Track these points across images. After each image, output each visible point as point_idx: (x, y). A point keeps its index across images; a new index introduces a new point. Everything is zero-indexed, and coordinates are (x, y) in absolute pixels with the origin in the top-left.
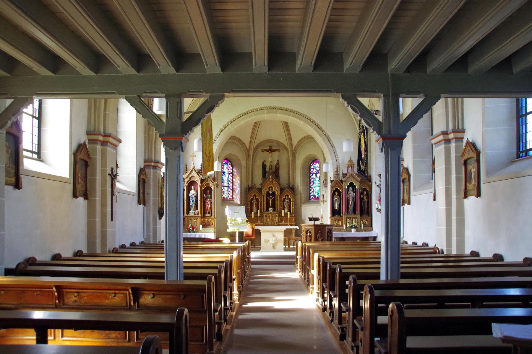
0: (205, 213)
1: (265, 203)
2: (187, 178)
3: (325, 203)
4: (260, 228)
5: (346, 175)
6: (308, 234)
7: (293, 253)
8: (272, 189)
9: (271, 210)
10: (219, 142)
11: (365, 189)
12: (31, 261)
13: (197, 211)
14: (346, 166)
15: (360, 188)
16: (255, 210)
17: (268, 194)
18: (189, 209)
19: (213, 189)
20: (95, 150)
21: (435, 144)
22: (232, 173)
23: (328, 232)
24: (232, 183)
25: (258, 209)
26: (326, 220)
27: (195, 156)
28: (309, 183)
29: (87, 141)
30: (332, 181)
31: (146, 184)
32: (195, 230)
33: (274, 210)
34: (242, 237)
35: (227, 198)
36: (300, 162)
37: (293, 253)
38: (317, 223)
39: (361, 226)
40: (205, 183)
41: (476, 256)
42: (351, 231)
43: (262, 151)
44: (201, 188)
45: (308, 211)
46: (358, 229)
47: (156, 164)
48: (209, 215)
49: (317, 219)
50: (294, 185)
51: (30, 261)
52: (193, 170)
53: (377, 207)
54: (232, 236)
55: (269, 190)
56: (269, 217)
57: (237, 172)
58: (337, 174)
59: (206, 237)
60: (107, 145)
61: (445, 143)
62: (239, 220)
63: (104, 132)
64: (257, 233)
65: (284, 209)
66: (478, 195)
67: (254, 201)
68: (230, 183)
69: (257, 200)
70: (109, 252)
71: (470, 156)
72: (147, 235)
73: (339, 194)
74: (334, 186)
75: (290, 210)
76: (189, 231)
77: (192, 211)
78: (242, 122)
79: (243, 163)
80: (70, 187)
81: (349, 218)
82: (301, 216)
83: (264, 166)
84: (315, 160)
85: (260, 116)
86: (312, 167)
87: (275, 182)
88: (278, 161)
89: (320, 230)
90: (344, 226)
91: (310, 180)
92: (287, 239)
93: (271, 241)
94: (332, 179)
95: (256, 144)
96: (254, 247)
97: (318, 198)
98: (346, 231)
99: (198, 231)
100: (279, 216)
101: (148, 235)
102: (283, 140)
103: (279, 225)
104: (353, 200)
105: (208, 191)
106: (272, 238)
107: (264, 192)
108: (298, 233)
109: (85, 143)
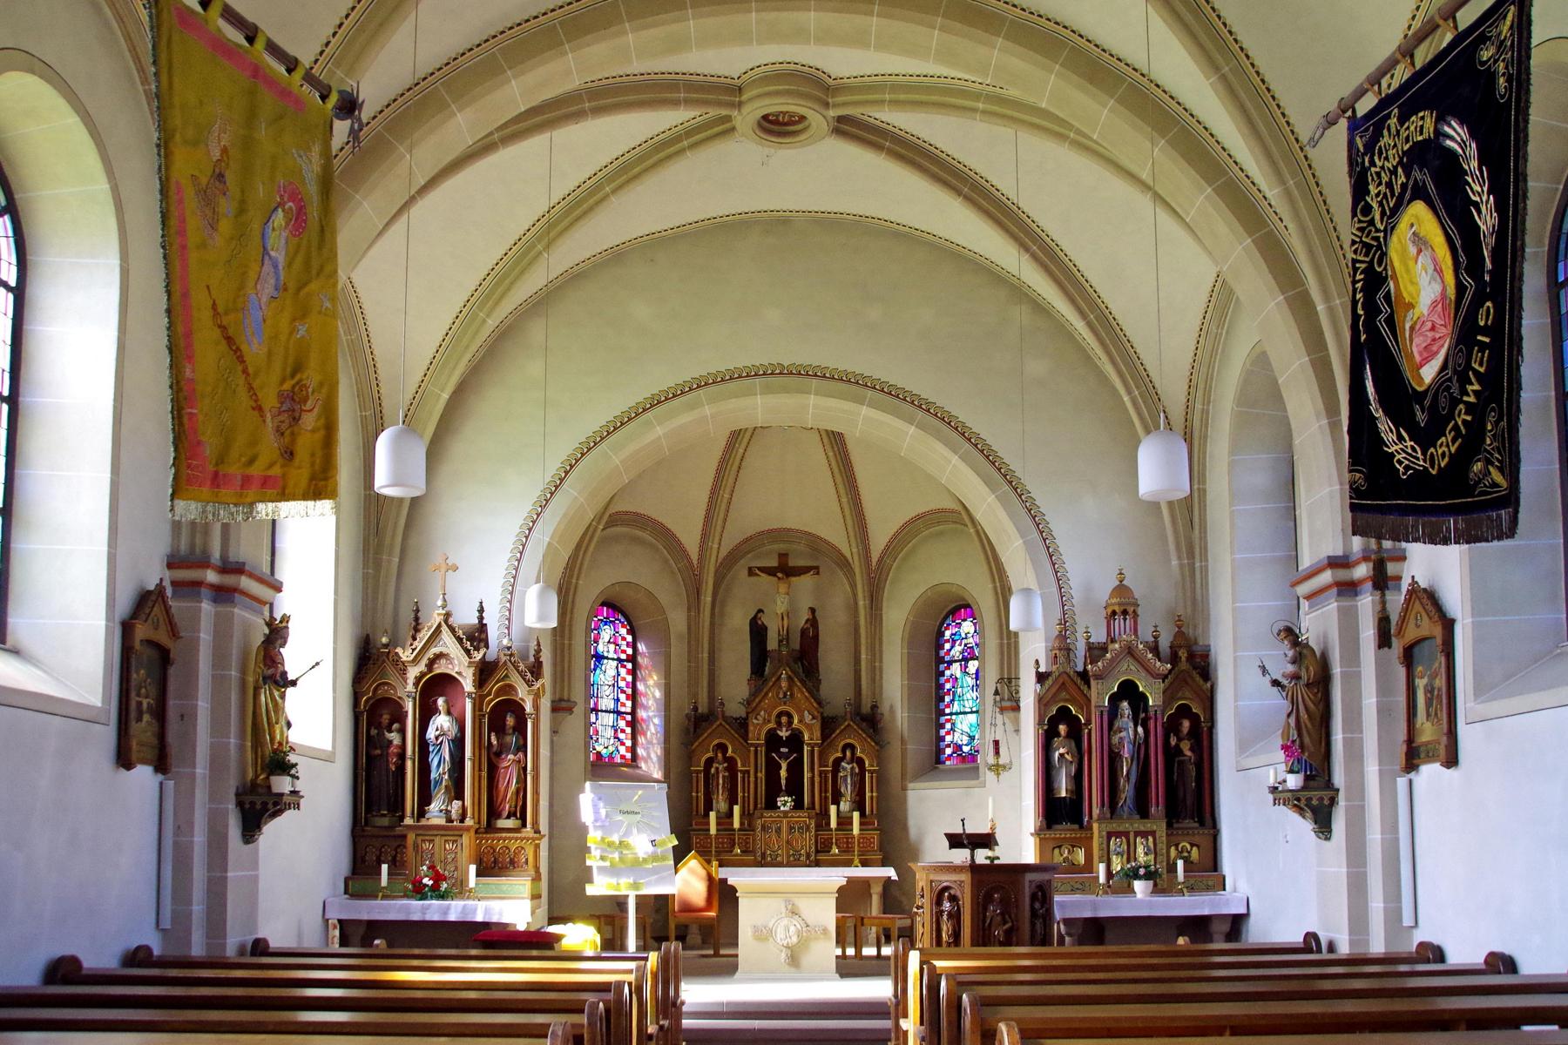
0: (494, 813)
1: (762, 775)
2: (415, 661)
3: (1004, 775)
4: (738, 878)
5: (1103, 649)
6: (947, 905)
7: (879, 989)
8: (790, 723)
9: (785, 802)
11: (1184, 711)
12: (63, 970)
13: (456, 804)
16: (721, 803)
17: (773, 741)
18: (425, 798)
19: (528, 708)
20: (195, 617)
21: (1308, 598)
22: (632, 659)
23: (1034, 897)
24: (634, 697)
25: (732, 801)
26: (1020, 843)
28: (934, 700)
29: (167, 584)
30: (1041, 678)
31: (172, 671)
32: (444, 886)
33: (798, 805)
34: (662, 920)
35: (611, 756)
36: (897, 616)
37: (879, 989)
38: (982, 856)
39: (1172, 869)
40: (494, 686)
41: (1435, 962)
42: (1131, 890)
43: (751, 572)
44: (477, 707)
45: (934, 812)
46: (1161, 881)
47: (229, 580)
48: (510, 823)
49: (987, 841)
50: (874, 707)
51: (141, 955)
52: (444, 628)
53: (1271, 782)
54: (609, 915)
55: (779, 724)
56: (779, 831)
57: (652, 656)
58: (1062, 647)
59: (495, 919)
60: (231, 602)
61: (1339, 594)
62: (641, 844)
63: (224, 558)
64: (723, 895)
65: (836, 802)
66: (1452, 761)
67: (720, 767)
68: (622, 697)
69: (731, 762)
70: (241, 951)
71: (1424, 632)
72: (174, 919)
73: (1075, 733)
74: (1053, 700)
75: (859, 805)
76: (419, 892)
77: (435, 806)
78: (658, 430)
79: (678, 620)
80: (107, 735)
81: (1118, 834)
82: (905, 828)
83: (758, 632)
84: (961, 608)
85: (733, 404)
86: (948, 634)
87: (801, 694)
88: (813, 610)
89: (996, 890)
90: (1102, 868)
91: (941, 686)
92: (850, 924)
93: (780, 934)
94: (1042, 669)
95: (724, 552)
96: (716, 955)
97: (972, 757)
98: (1109, 889)
99: (460, 890)
100: (818, 827)
101: (182, 919)
102: (835, 532)
103: (817, 864)
104: (1139, 748)
106: (785, 922)
107: (757, 734)
108: (894, 897)
109: (160, 588)
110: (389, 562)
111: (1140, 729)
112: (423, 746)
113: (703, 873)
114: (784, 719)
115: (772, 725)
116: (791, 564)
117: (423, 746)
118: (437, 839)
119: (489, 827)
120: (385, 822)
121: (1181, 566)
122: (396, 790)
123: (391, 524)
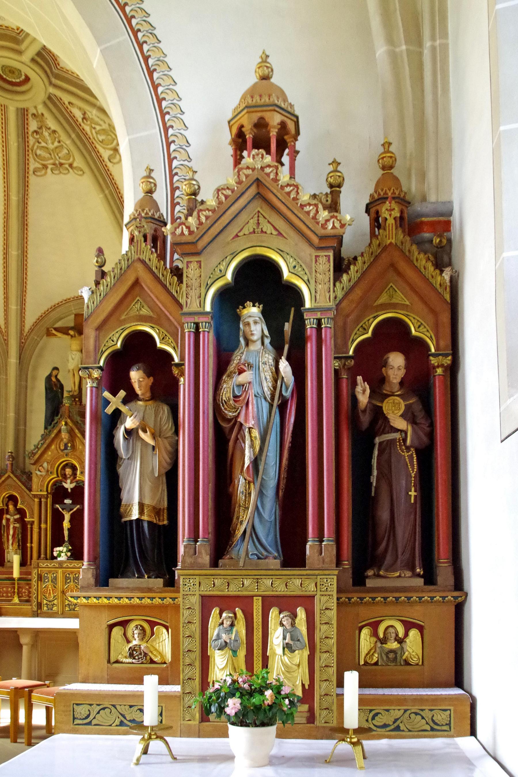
8: (74, 474)
11: (394, 334)
14: (226, 137)
15: (345, 318)
17: (58, 493)
56: (54, 580)
81: (226, 603)
111: (284, 366)
114: (68, 471)
121: (394, 58)
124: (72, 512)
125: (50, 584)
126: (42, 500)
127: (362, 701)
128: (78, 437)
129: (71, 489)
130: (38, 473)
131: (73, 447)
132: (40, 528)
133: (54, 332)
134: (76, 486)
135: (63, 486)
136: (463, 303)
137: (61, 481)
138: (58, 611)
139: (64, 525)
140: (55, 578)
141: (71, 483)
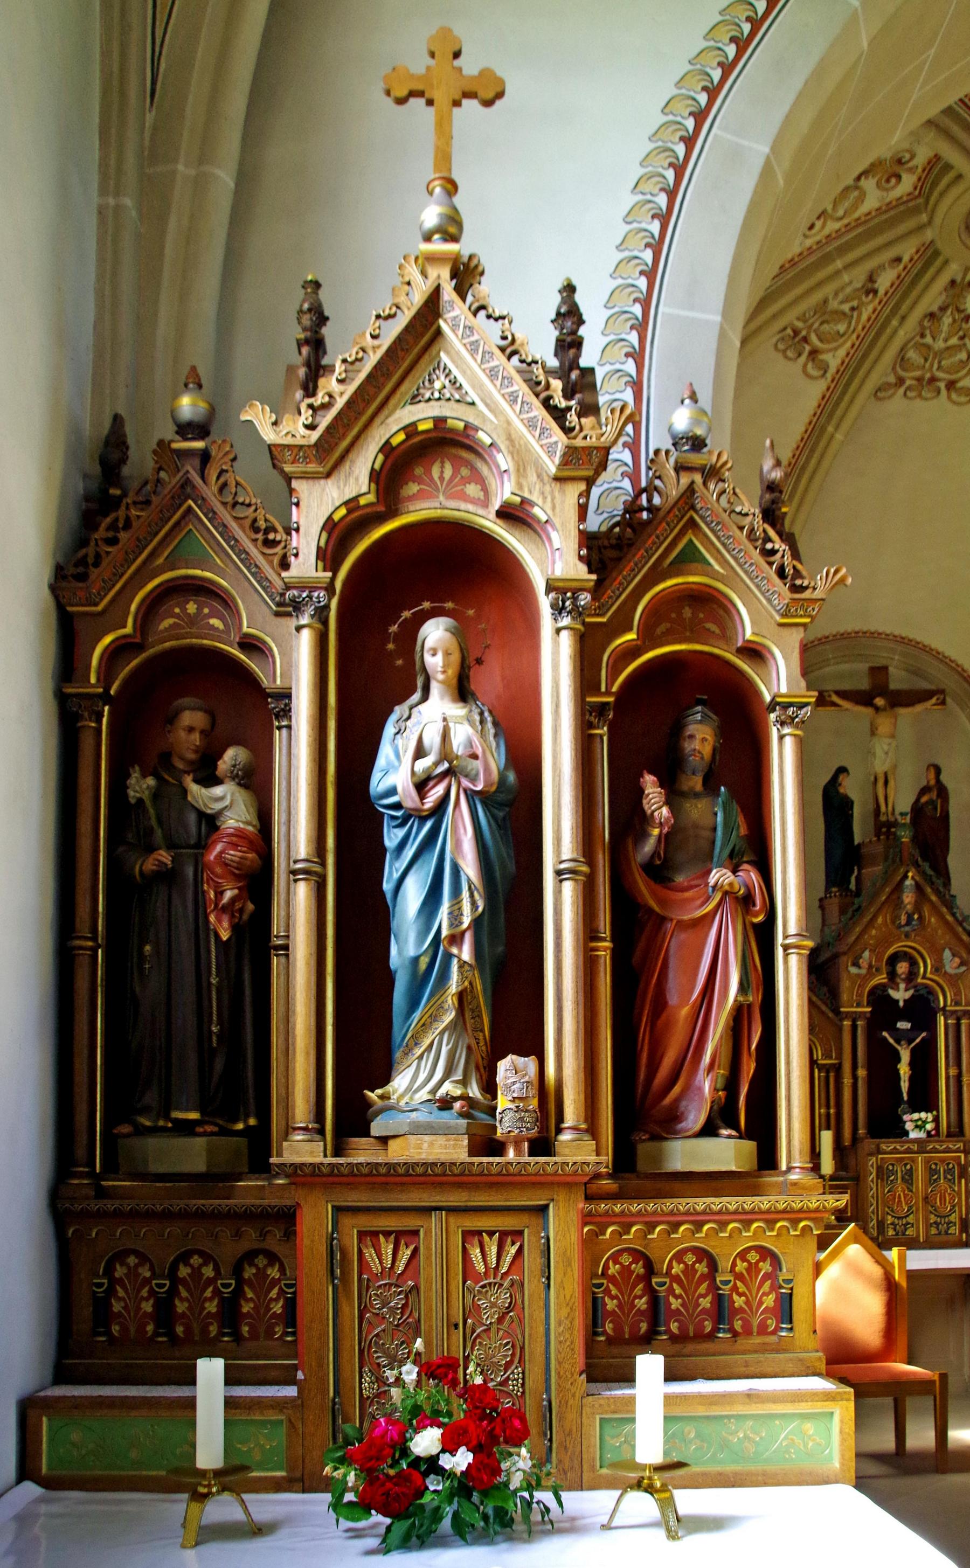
8: (911, 976)
9: (916, 1125)
10: (745, 185)
13: (512, 1071)
18: (365, 1053)
27: (490, 94)
48: (727, 1152)
55: (892, 975)
56: (909, 1178)
77: (417, 1083)
105: (701, 737)
110: (200, 184)
112: (355, 819)
113: (877, 1271)
115: (881, 978)
116: (893, 686)
117: (355, 819)
118: (433, 1229)
119: (633, 1160)
120: (193, 1154)
122: (232, 1033)
123: (203, 53)
124: (913, 1045)
125: (900, 1188)
126: (859, 1023)
127: (230, 1404)
128: (930, 901)
129: (905, 1001)
130: (853, 970)
131: (921, 918)
132: (855, 1077)
133: (835, 698)
134: (913, 996)
135: (889, 996)
136: (311, 668)
137: (883, 987)
138: (918, 1236)
139: (902, 1072)
140: (910, 1173)
141: (906, 990)
